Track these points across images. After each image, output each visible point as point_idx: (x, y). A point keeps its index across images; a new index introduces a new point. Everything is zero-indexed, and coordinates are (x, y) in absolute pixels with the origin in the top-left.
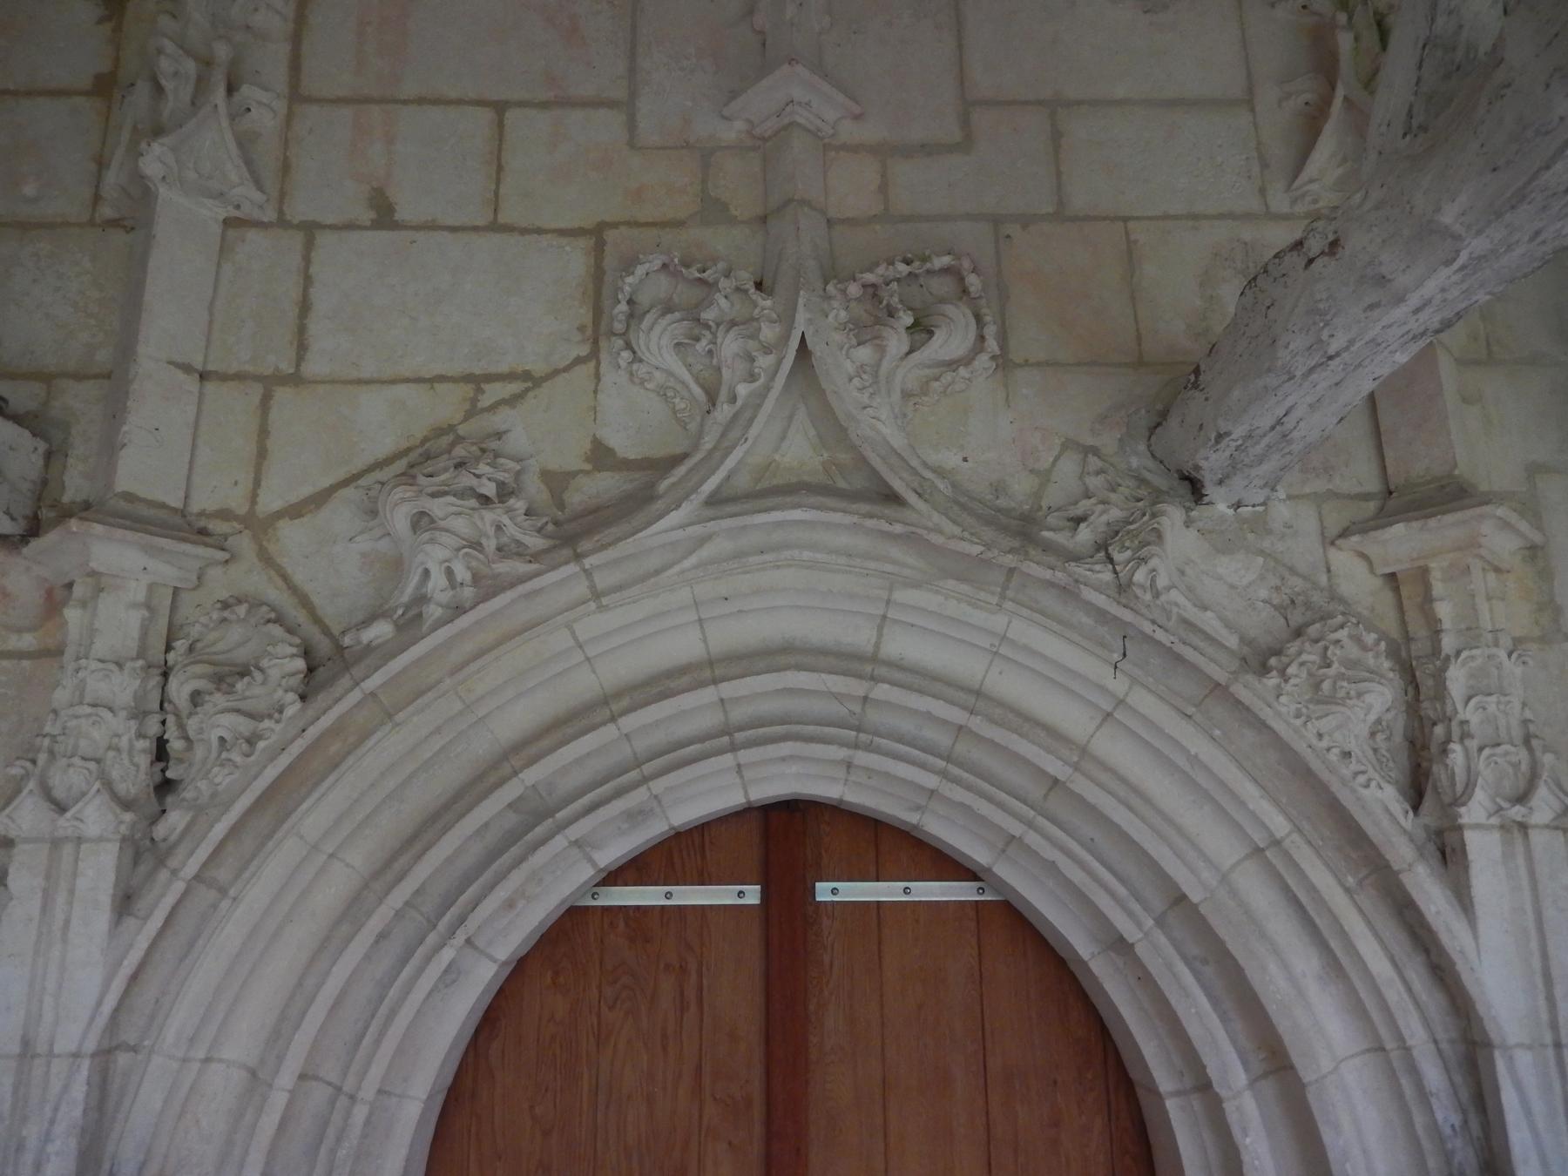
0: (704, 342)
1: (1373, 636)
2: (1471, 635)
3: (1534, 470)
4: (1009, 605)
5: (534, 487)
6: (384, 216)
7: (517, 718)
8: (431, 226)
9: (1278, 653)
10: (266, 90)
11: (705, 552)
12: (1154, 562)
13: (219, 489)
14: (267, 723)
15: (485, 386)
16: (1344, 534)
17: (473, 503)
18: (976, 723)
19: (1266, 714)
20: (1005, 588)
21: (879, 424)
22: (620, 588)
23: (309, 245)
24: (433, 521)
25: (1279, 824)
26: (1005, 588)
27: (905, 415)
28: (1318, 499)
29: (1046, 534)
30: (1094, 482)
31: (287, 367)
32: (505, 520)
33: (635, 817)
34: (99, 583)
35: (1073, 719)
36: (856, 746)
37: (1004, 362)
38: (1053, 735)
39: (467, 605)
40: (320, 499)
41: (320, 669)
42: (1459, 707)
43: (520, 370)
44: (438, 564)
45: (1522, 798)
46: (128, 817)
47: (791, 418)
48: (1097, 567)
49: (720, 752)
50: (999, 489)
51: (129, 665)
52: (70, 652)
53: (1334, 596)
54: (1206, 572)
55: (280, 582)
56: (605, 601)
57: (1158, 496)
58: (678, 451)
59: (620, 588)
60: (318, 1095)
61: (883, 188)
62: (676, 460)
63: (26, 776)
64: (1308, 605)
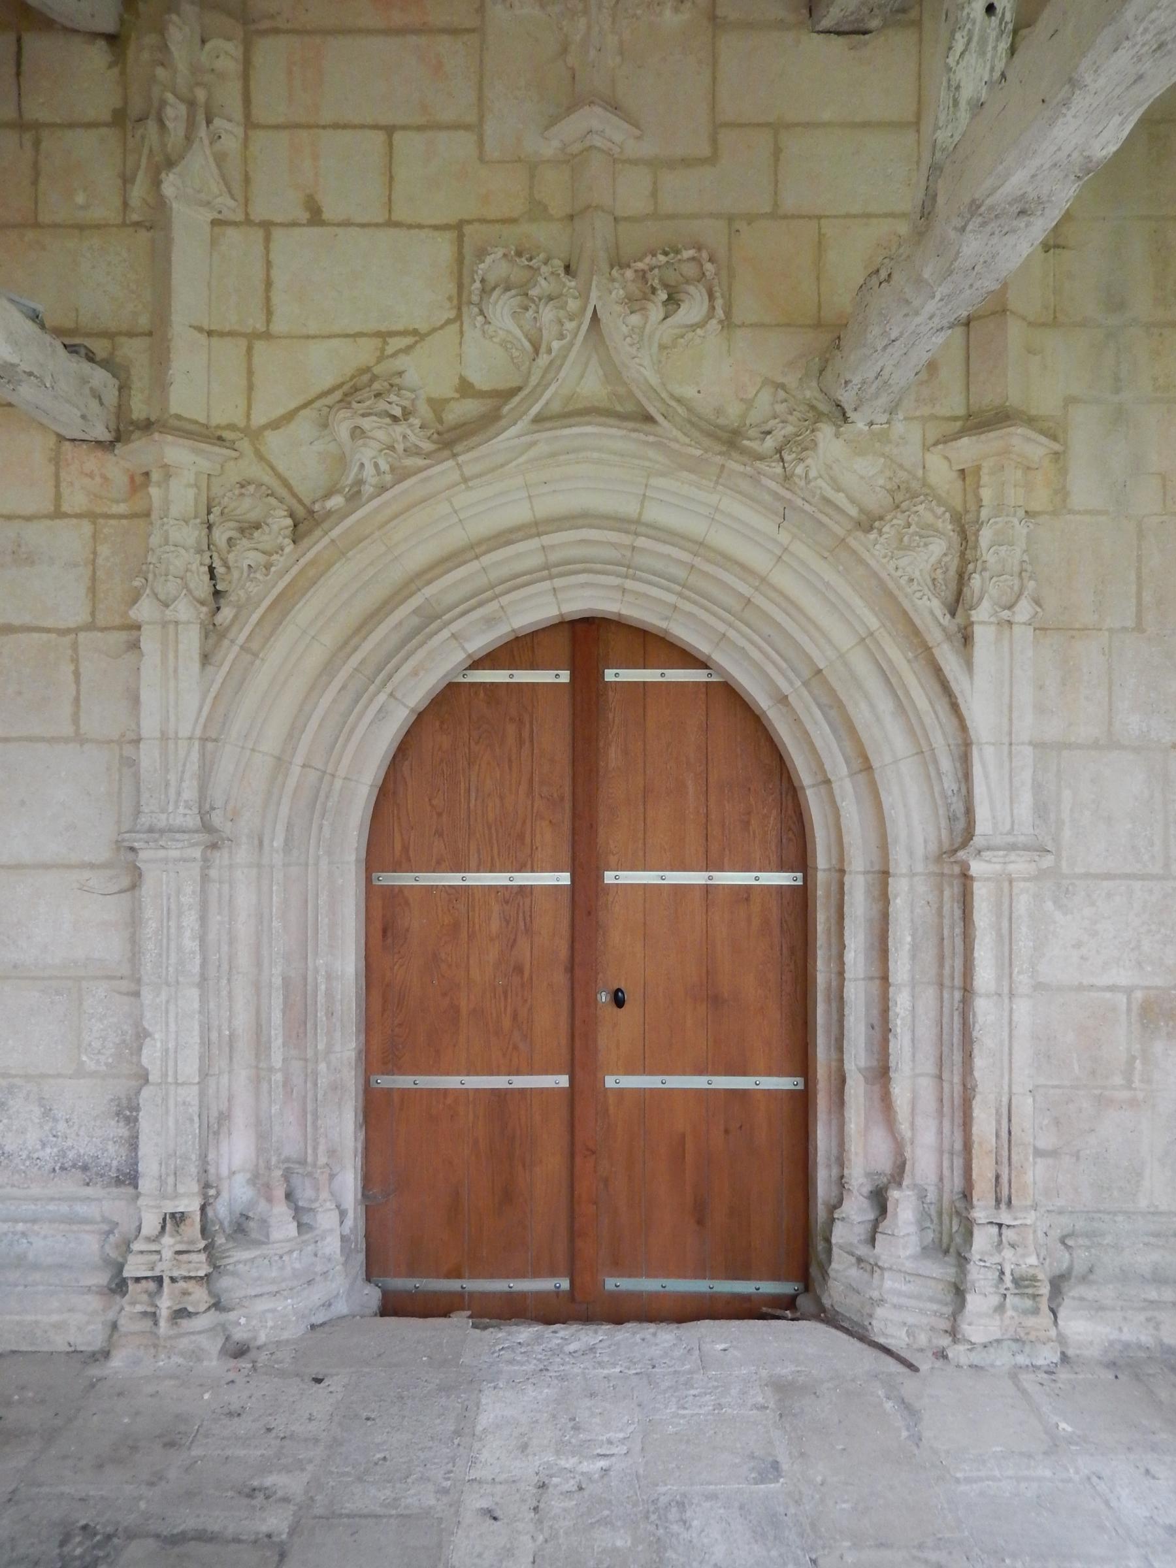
0: (531, 312)
1: (943, 509)
2: (1000, 508)
3: (1070, 401)
4: (720, 488)
5: (424, 409)
6: (316, 217)
7: (419, 557)
8: (347, 224)
9: (881, 518)
10: (230, 120)
11: (532, 453)
12: (809, 461)
13: (227, 412)
14: (275, 557)
15: (389, 340)
16: (935, 444)
17: (388, 420)
18: (697, 561)
19: (866, 556)
20: (719, 477)
21: (643, 369)
22: (479, 475)
23: (267, 239)
24: (363, 432)
25: (873, 622)
26: (719, 477)
27: (660, 362)
28: (924, 420)
29: (745, 442)
30: (780, 408)
31: (261, 327)
32: (409, 432)
33: (490, 621)
34: (168, 472)
35: (758, 559)
36: (626, 577)
37: (728, 324)
38: (745, 570)
39: (389, 486)
40: (290, 416)
41: (303, 524)
42: (984, 552)
43: (411, 328)
44: (369, 460)
45: (1010, 607)
46: (204, 609)
47: (586, 364)
48: (773, 464)
49: (543, 579)
50: (719, 411)
51: (192, 521)
52: (155, 516)
53: (925, 484)
54: (843, 465)
55: (270, 472)
56: (470, 484)
57: (819, 416)
58: (515, 384)
59: (479, 475)
60: (313, 776)
61: (654, 194)
62: (514, 392)
63: (144, 587)
64: (908, 490)
